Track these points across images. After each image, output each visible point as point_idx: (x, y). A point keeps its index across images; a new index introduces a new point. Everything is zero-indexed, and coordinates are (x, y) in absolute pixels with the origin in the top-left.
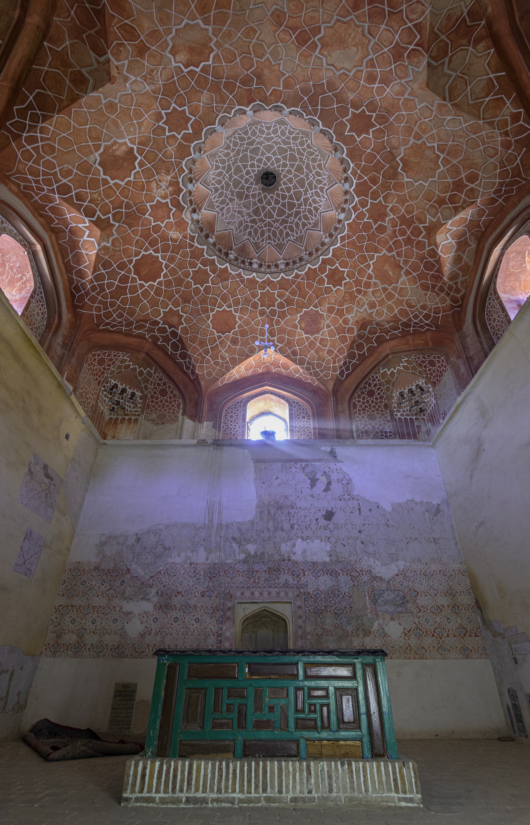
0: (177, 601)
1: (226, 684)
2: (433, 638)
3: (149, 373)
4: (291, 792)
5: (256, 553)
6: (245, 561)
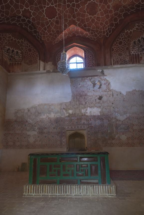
0: (45, 131)
1: (53, 164)
2: (138, 140)
3: (22, 42)
4: (74, 193)
5: (72, 113)
6: (68, 116)
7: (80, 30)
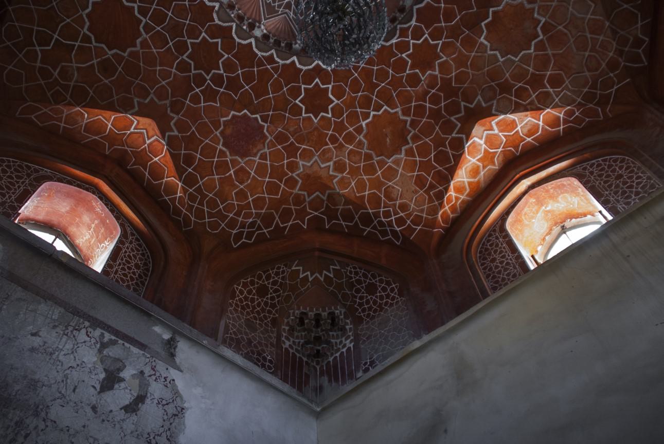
7: (162, 158)
